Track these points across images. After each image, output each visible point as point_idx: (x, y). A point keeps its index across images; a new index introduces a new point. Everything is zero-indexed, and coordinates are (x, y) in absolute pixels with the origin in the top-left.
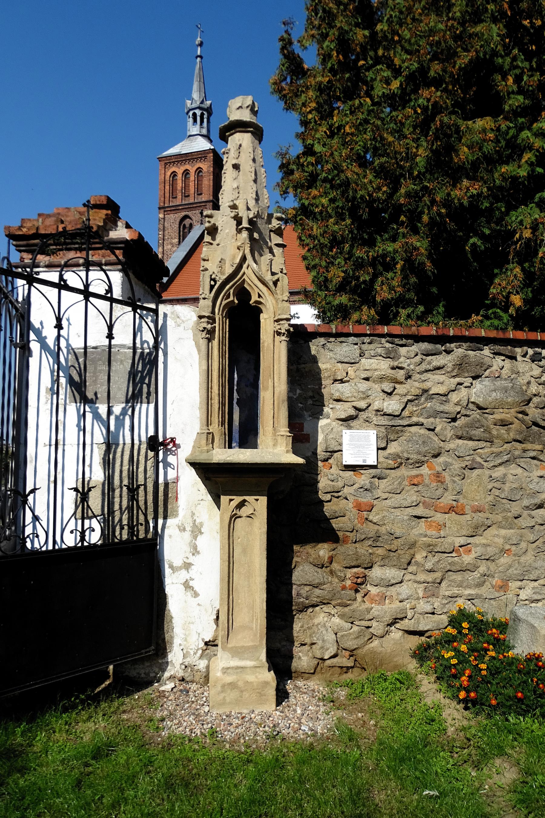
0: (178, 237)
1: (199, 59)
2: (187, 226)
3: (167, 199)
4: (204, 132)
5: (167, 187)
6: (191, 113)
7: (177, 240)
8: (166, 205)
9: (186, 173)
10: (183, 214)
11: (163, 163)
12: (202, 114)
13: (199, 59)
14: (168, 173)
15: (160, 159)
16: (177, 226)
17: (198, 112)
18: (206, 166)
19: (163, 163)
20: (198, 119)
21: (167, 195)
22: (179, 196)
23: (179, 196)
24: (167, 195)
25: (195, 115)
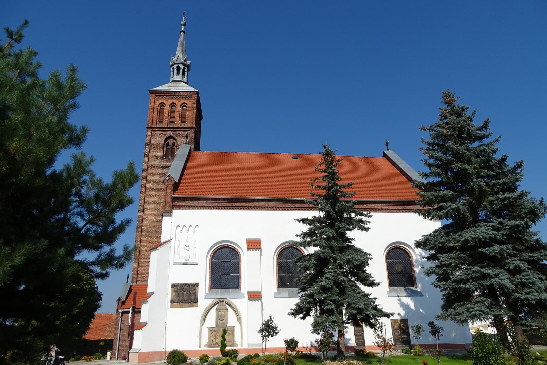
0: (162, 152)
1: (182, 33)
2: (171, 144)
4: (185, 80)
5: (156, 113)
6: (175, 66)
7: (161, 154)
8: (153, 126)
9: (173, 105)
11: (153, 95)
12: (184, 69)
13: (182, 33)
14: (158, 103)
15: (151, 92)
16: (162, 143)
17: (182, 66)
18: (191, 103)
19: (153, 95)
20: (181, 70)
21: (155, 119)
22: (166, 121)
23: (166, 121)
24: (155, 119)
25: (178, 68)
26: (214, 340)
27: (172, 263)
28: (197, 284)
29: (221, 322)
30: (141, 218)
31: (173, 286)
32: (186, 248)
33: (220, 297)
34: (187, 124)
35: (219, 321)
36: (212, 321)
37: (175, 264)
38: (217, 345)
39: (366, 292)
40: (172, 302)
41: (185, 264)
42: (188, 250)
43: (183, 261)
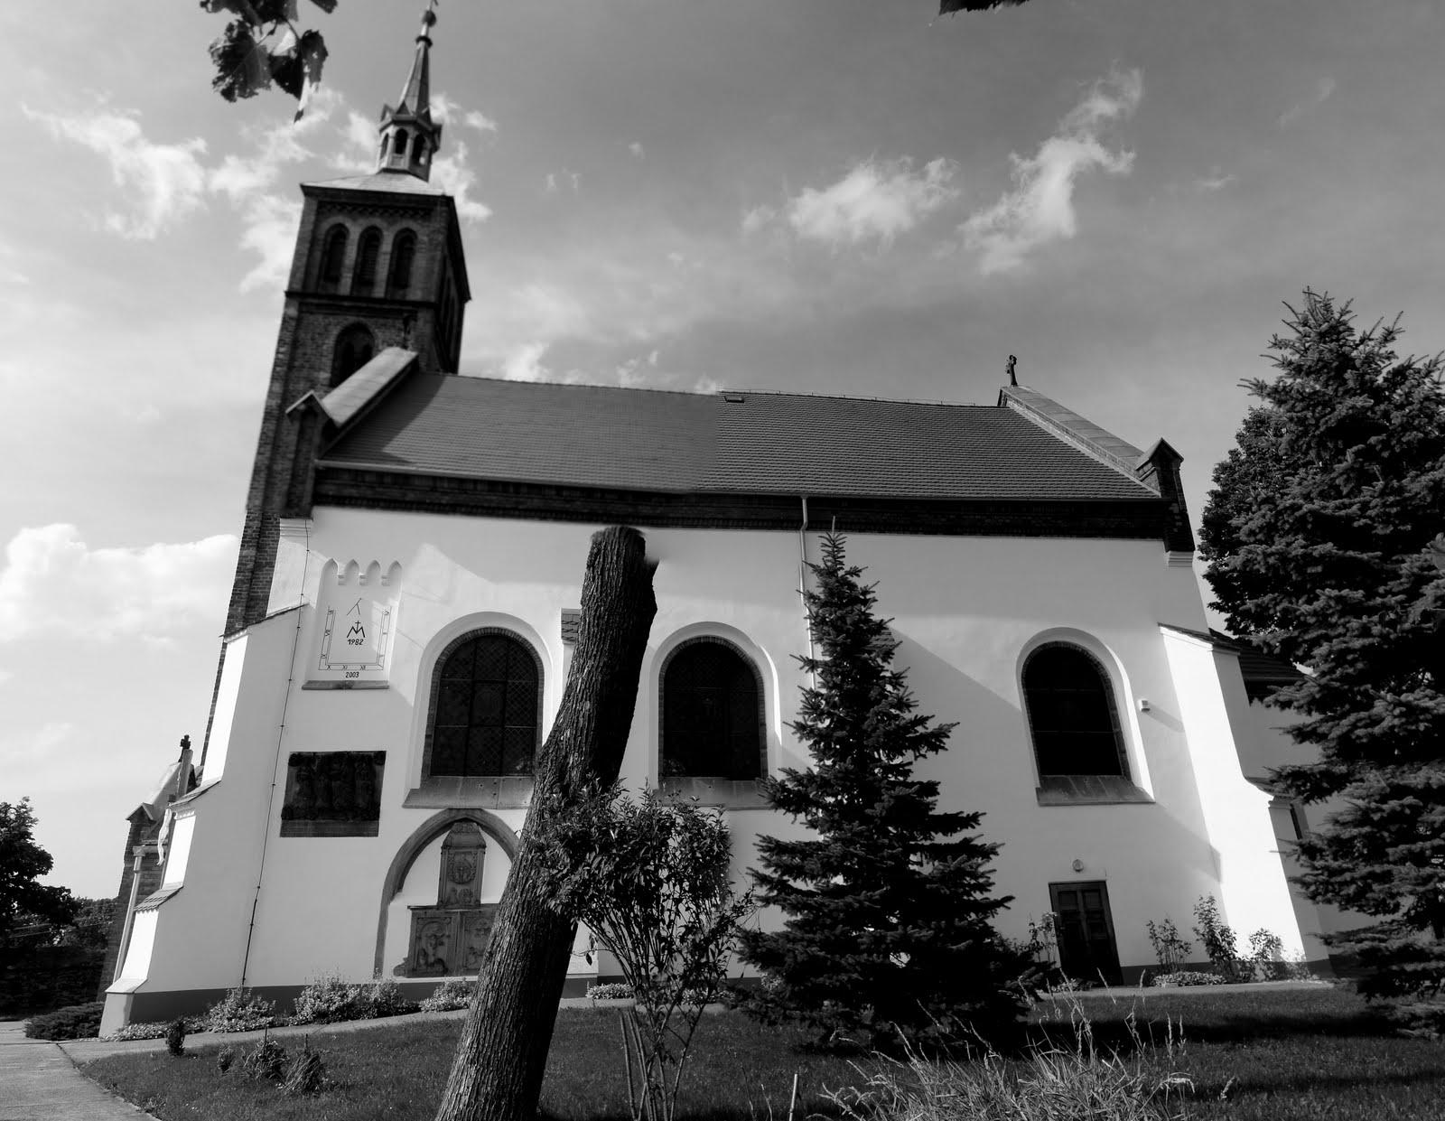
3: (313, 281)
5: (318, 255)
10: (351, 319)
24: (315, 271)
26: (430, 951)
27: (301, 682)
28: (380, 757)
29: (459, 888)
30: (250, 566)
31: (297, 760)
32: (353, 636)
33: (459, 801)
34: (416, 293)
35: (450, 885)
36: (425, 887)
37: (311, 686)
38: (439, 968)
39: (1353, 911)
40: (289, 814)
41: (341, 686)
42: (358, 642)
43: (341, 676)
